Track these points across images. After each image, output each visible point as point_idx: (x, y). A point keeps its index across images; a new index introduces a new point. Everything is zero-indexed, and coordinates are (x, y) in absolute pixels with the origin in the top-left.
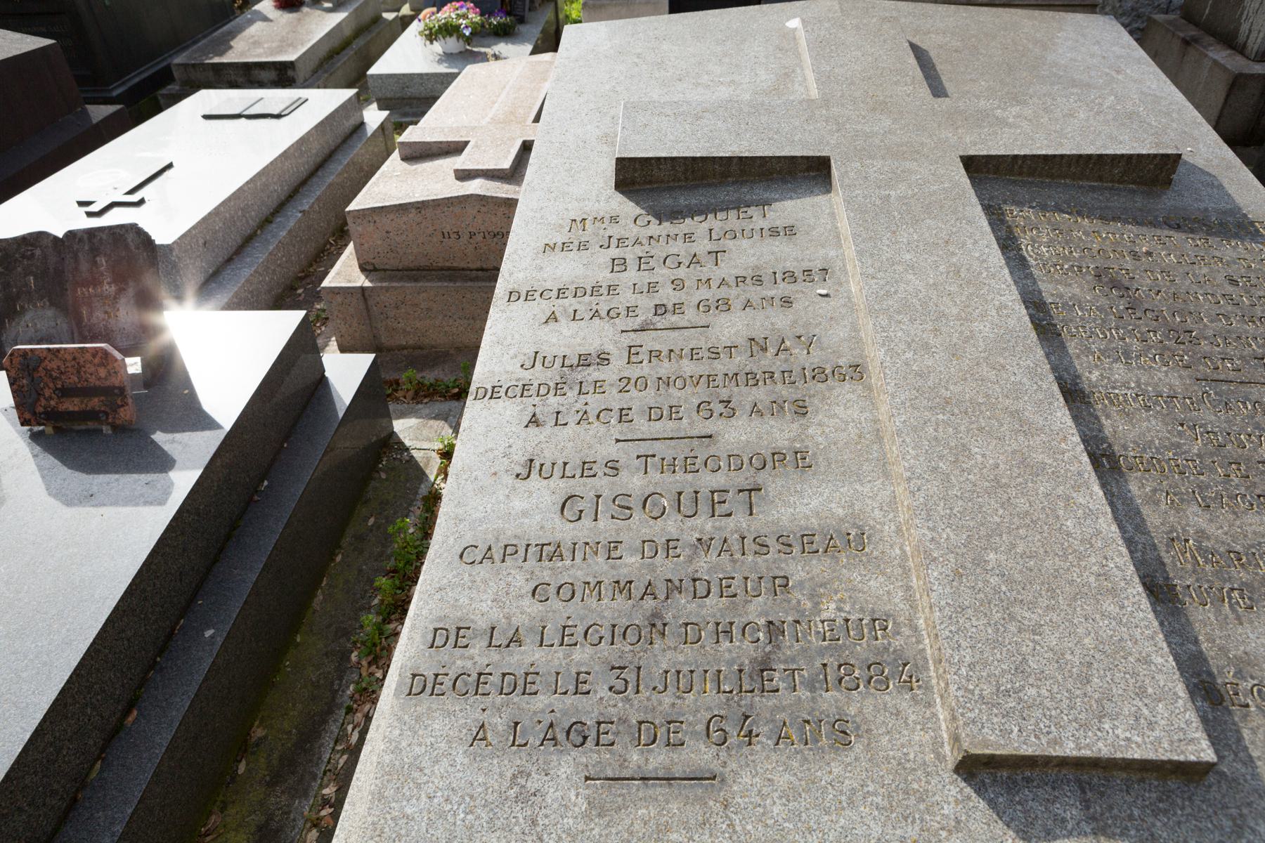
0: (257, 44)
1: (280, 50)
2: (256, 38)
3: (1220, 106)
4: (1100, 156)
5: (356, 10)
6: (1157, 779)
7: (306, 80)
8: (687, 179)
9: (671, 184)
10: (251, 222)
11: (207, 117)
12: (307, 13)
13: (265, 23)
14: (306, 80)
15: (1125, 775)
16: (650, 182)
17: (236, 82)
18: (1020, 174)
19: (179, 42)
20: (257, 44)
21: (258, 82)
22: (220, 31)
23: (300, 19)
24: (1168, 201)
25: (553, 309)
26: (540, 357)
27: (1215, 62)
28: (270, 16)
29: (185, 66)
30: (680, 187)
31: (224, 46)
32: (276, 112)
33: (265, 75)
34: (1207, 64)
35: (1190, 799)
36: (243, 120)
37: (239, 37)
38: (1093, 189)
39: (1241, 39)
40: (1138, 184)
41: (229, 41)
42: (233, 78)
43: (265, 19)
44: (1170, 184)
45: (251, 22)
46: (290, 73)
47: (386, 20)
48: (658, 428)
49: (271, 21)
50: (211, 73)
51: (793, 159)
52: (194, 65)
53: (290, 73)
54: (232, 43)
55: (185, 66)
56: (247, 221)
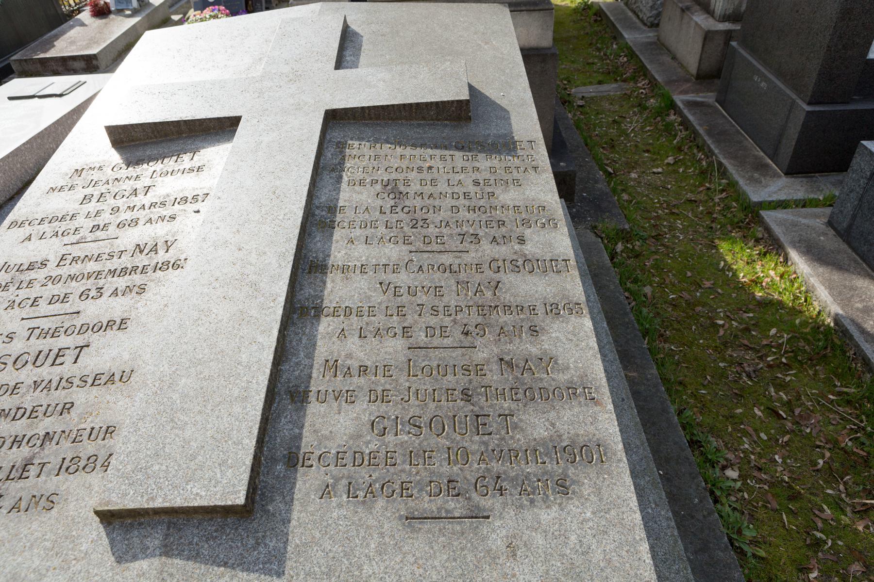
0: (73, 43)
1: (88, 46)
2: (73, 39)
3: (700, 52)
4: (418, 104)
5: (148, 15)
6: (222, 518)
7: (107, 67)
8: (156, 137)
9: (147, 141)
10: (29, 171)
11: (11, 98)
12: (113, 18)
13: (82, 28)
14: (107, 67)
15: (201, 517)
16: (133, 141)
17: (57, 70)
18: (371, 119)
19: (21, 43)
20: (73, 43)
21: (73, 70)
22: (49, 35)
23: (106, 24)
24: (476, 130)
25: (32, 232)
26: (7, 266)
27: (696, 23)
28: (86, 22)
29: (20, 61)
30: (152, 143)
31: (50, 45)
32: (58, 93)
33: (77, 65)
34: (693, 24)
35: (237, 529)
36: (37, 98)
37: (62, 38)
38: (419, 125)
39: (712, 7)
40: (450, 120)
41: (54, 41)
42: (55, 68)
43: (83, 24)
44: (470, 119)
45: (72, 27)
46: (94, 62)
47: (173, 20)
48: (57, 308)
49: (86, 26)
50: (39, 65)
51: (219, 120)
52: (26, 60)
53: (94, 62)
54: (55, 43)
55: (20, 61)
56: (26, 171)
